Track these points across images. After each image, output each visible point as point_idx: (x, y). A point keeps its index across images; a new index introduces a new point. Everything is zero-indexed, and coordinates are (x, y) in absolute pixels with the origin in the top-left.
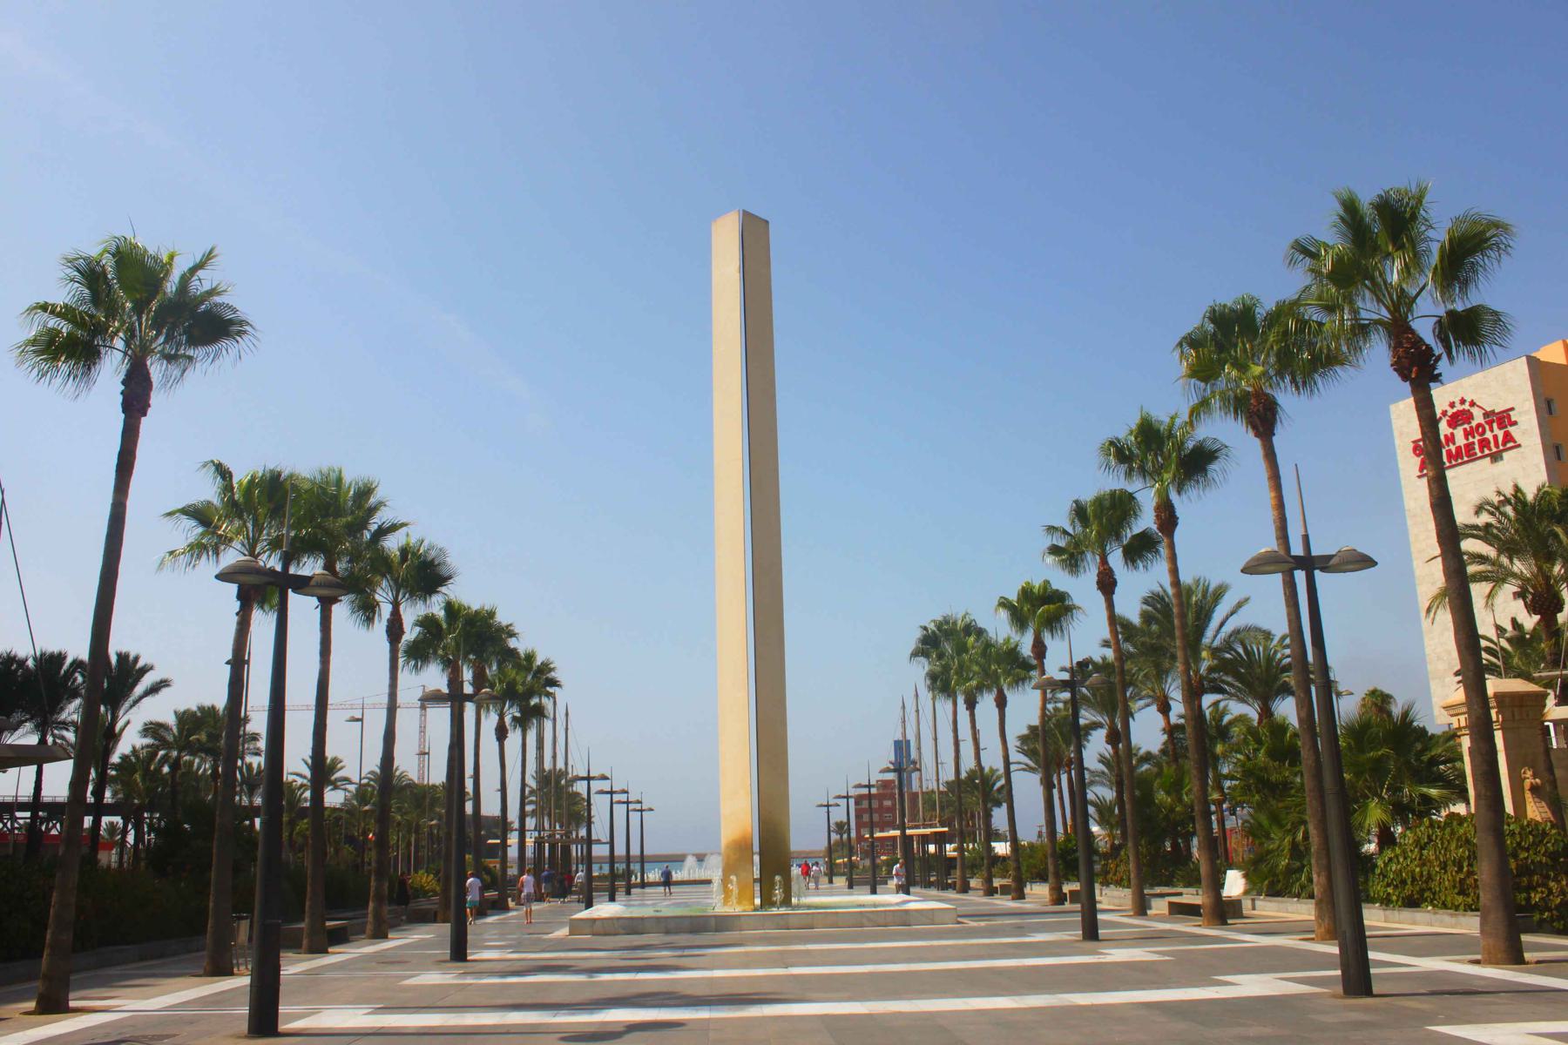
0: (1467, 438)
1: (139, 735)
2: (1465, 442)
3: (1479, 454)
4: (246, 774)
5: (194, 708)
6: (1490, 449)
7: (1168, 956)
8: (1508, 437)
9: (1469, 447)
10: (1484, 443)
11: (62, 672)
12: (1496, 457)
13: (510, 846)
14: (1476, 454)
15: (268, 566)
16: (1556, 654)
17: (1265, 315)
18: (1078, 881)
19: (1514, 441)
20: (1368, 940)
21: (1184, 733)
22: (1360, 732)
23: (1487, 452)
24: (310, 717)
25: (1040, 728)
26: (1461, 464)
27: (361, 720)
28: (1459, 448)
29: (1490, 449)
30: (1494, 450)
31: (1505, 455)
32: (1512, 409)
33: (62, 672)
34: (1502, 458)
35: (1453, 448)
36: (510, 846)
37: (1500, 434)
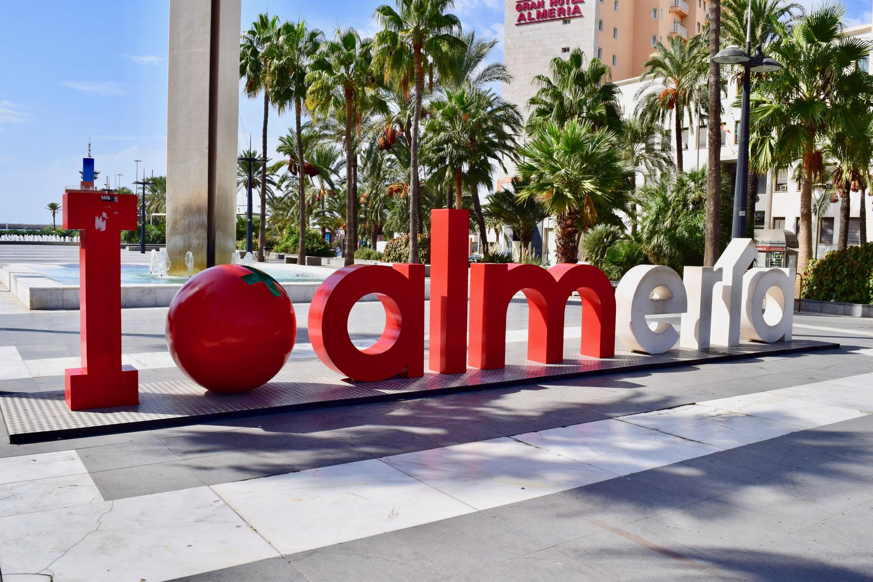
0: (551, 6)
1: (252, 99)
2: (550, 8)
3: (558, 17)
7: (413, 435)
8: (577, 10)
9: (552, 11)
10: (562, 11)
11: (242, 340)
12: (566, 21)
14: (555, 16)
18: (441, 373)
19: (580, 13)
20: (123, 337)
23: (562, 17)
24: (769, 214)
25: (91, 189)
26: (544, 21)
27: (797, 274)
28: (545, 11)
30: (567, 16)
31: (572, 21)
33: (242, 340)
34: (569, 22)
35: (541, 10)
37: (572, 6)
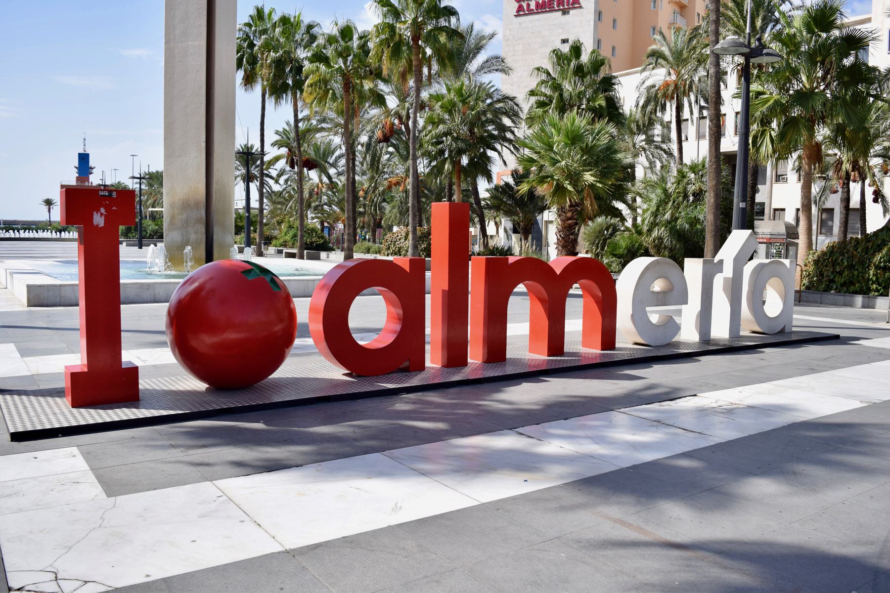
4: (440, 426)
5: (154, 172)
6: (563, 6)
13: (256, 201)
14: (554, 7)
15: (152, 246)
16: (725, 199)
17: (376, 4)
19: (579, 4)
21: (445, 151)
22: (253, 179)
23: (561, 8)
25: (86, 184)
26: (543, 12)
29: (563, 6)
30: (566, 7)
31: (571, 12)
32: (515, 16)
34: (568, 13)
36: (256, 201)
